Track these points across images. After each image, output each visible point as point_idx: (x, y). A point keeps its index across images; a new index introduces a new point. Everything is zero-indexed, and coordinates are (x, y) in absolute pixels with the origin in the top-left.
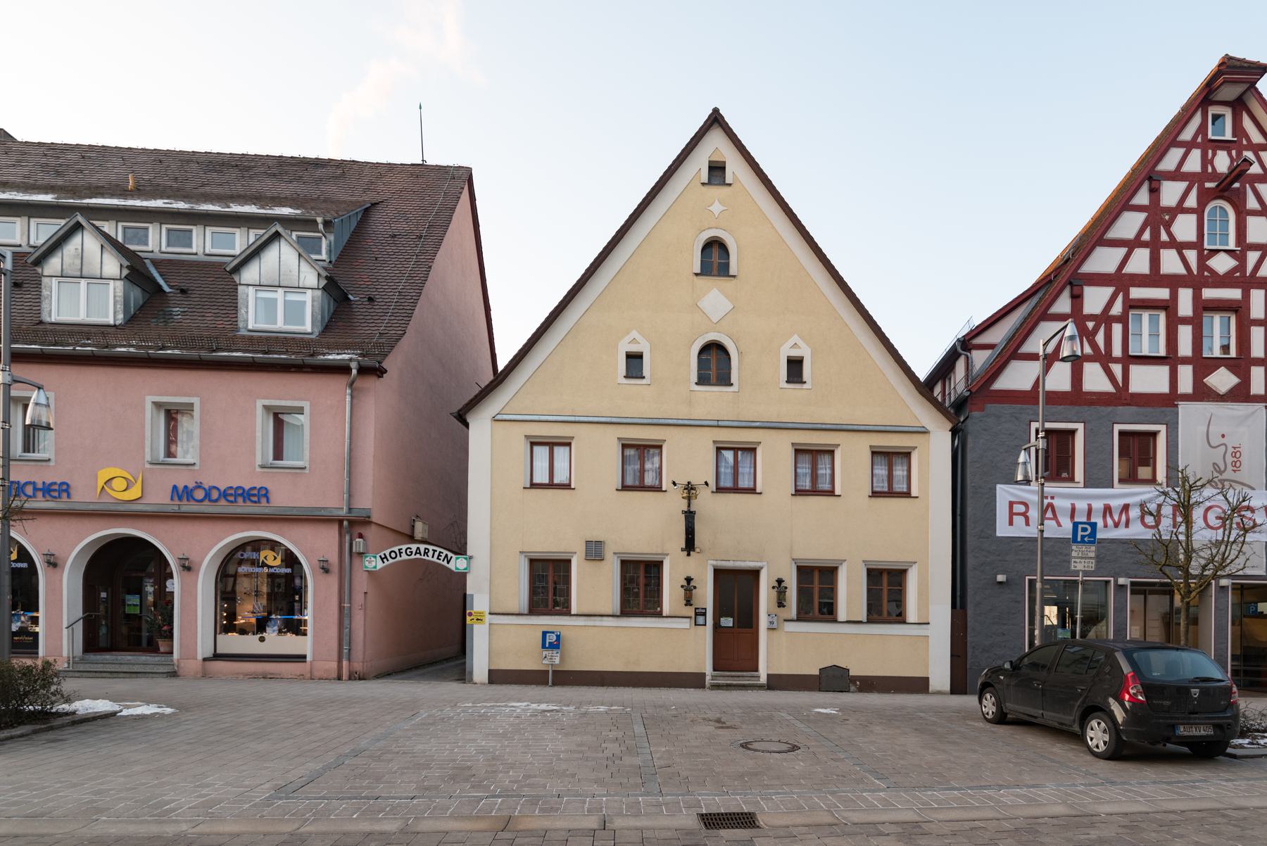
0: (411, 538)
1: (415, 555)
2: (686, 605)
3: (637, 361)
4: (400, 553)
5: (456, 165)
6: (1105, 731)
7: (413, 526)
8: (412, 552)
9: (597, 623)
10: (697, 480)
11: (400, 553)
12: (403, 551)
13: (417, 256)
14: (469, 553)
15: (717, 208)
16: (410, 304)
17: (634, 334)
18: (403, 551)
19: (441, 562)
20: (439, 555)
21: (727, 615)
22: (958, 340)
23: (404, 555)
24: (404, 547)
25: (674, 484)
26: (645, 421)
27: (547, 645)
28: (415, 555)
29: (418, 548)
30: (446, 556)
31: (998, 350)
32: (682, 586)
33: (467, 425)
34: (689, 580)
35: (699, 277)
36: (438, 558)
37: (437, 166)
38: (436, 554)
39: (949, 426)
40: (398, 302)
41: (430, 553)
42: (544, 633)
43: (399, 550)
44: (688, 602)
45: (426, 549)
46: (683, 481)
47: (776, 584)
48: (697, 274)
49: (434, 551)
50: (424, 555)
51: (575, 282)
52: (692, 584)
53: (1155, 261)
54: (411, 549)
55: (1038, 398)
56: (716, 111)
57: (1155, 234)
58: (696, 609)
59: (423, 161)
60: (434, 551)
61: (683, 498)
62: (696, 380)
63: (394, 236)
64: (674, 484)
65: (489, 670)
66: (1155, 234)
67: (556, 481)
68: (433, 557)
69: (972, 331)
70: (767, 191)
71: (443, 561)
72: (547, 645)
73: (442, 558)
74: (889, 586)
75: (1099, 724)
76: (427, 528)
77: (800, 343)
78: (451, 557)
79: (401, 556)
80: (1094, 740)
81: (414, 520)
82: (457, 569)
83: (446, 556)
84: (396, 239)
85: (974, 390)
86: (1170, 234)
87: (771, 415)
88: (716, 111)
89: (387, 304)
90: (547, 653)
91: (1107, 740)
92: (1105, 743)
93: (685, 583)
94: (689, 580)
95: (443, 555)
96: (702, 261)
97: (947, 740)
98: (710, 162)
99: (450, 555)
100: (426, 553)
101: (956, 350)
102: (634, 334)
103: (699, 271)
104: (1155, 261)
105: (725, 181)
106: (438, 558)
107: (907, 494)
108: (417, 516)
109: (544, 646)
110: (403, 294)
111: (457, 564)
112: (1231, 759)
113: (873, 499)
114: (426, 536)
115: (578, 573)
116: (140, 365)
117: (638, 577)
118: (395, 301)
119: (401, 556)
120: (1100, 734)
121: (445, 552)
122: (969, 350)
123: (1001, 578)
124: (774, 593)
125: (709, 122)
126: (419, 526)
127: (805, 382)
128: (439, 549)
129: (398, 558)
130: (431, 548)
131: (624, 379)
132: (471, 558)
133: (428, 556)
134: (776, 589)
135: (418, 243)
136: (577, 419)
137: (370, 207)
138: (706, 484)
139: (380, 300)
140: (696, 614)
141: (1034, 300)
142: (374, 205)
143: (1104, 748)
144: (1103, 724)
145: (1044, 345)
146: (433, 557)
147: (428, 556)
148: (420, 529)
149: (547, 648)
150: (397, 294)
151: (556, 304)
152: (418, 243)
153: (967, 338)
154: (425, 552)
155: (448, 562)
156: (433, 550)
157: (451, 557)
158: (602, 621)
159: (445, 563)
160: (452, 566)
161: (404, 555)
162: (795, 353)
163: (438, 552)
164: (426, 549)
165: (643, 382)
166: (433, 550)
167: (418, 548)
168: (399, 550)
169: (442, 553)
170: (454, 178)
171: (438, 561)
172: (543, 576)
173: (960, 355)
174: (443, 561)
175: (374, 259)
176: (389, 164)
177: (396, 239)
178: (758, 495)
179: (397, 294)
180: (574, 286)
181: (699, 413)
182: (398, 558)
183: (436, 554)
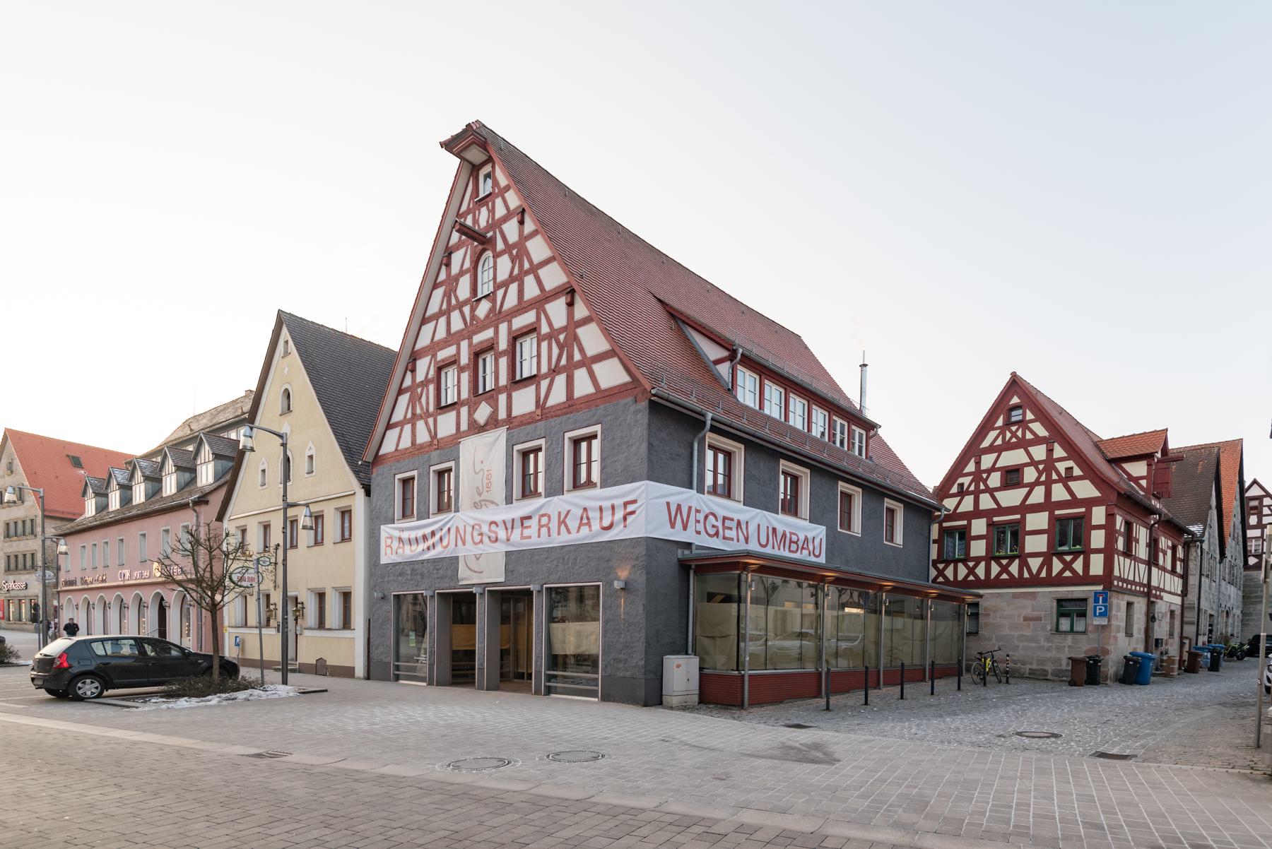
6: (84, 683)
53: (1048, 493)
57: (977, 486)
66: (977, 486)
67: (1184, 625)
75: (80, 688)
80: (93, 691)
86: (986, 485)
91: (89, 680)
92: (92, 683)
97: (61, 802)
104: (1048, 493)
112: (1237, 474)
116: (773, 380)
120: (87, 687)
141: (698, 626)
143: (97, 683)
144: (80, 685)
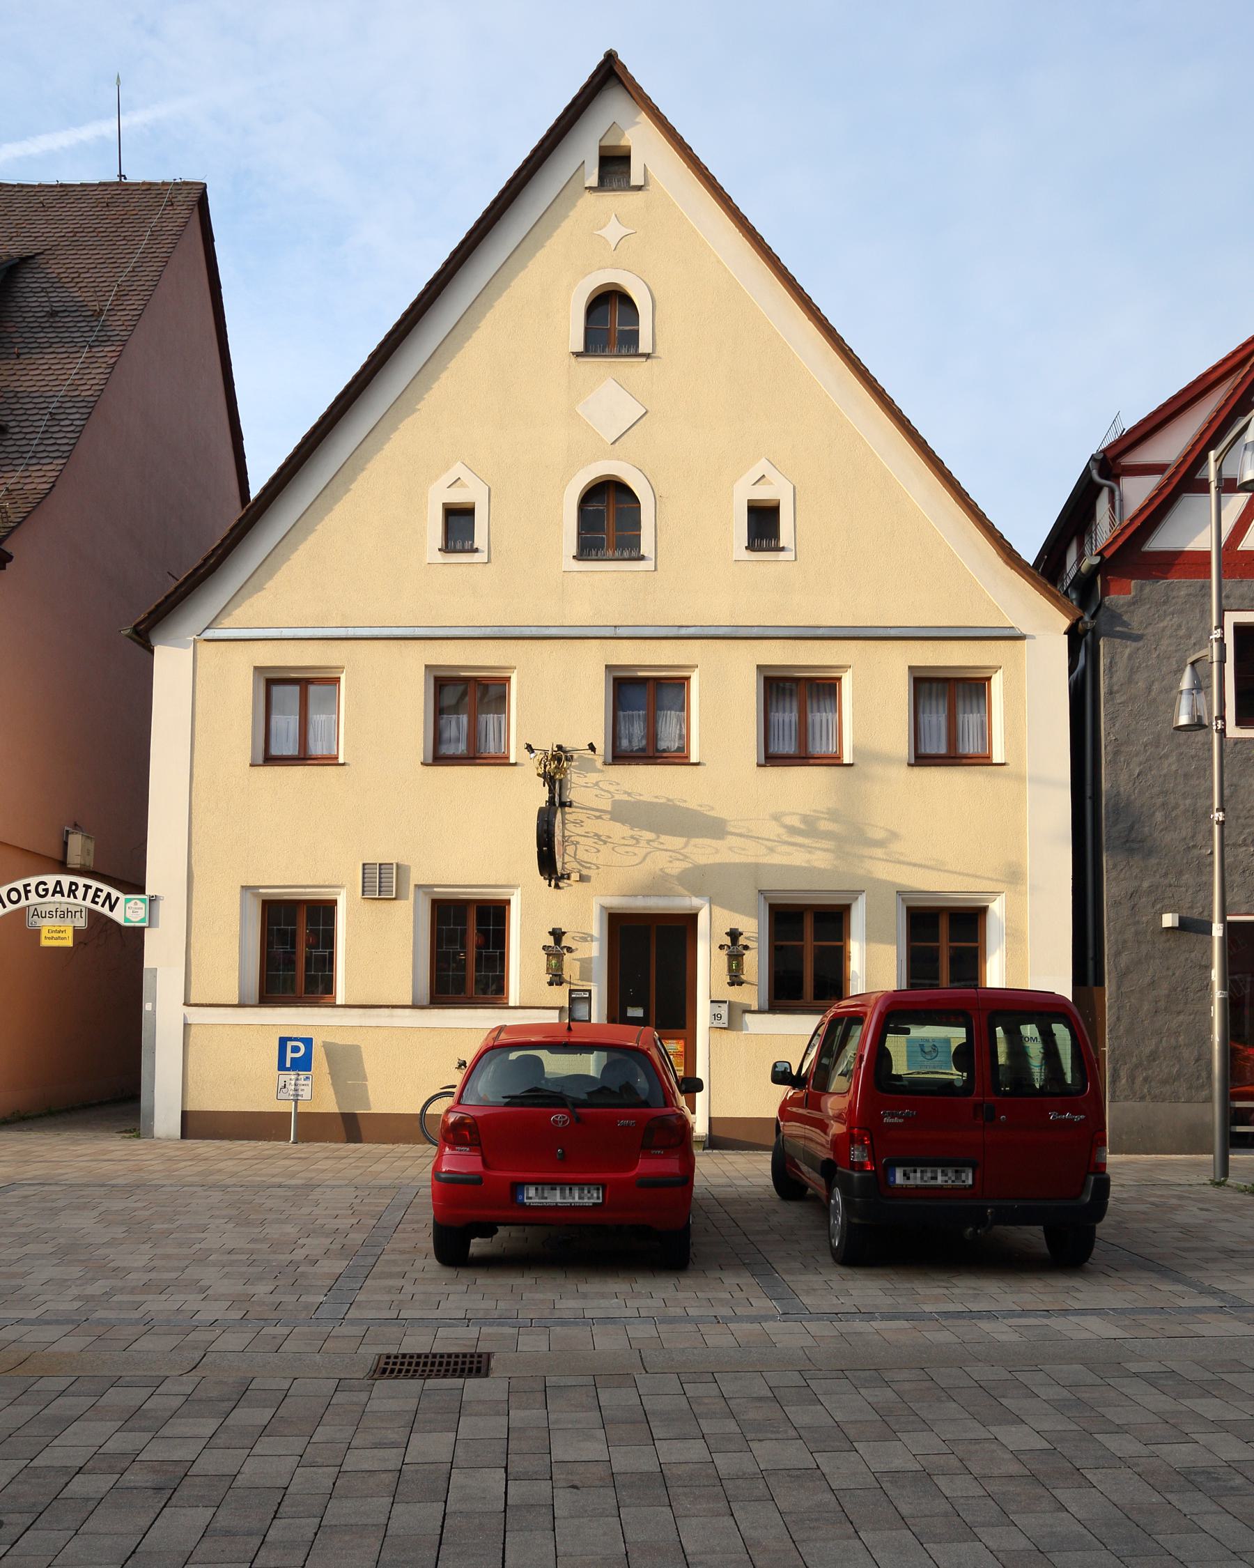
0: (62, 866)
1: (53, 895)
2: (731, 984)
3: (463, 520)
4: (27, 892)
5: (179, 181)
7: (66, 844)
8: (46, 890)
9: (397, 1022)
10: (575, 741)
11: (27, 892)
12: (32, 888)
13: (91, 347)
14: (150, 890)
15: (613, 231)
16: (69, 435)
17: (458, 470)
18: (32, 888)
19: (98, 908)
20: (96, 896)
21: (635, 1005)
22: (1093, 458)
23: (32, 895)
24: (33, 881)
25: (530, 748)
26: (477, 633)
27: (288, 1065)
28: (53, 895)
29: (58, 883)
30: (109, 896)
31: (1168, 473)
32: (544, 948)
33: (152, 652)
34: (557, 935)
35: (580, 359)
36: (93, 901)
37: (144, 184)
38: (91, 893)
39: (1065, 623)
40: (47, 431)
41: (81, 891)
42: (283, 1042)
43: (25, 886)
44: (557, 979)
45: (72, 884)
46: (546, 744)
47: (727, 941)
48: (578, 355)
49: (87, 887)
50: (69, 896)
51: (348, 379)
52: (742, 941)
54: (45, 884)
55: (1210, 563)
56: (611, 57)
58: (571, 991)
59: (120, 176)
60: (87, 887)
61: (539, 775)
62: (574, 551)
63: (53, 314)
64: (530, 748)
65: (184, 1114)
68: (84, 899)
69: (1122, 438)
70: (540, 169)
71: (103, 905)
72: (288, 1065)
73: (100, 900)
74: (951, 941)
76: (91, 846)
77: (772, 474)
78: (118, 899)
79: (27, 898)
81: (67, 831)
82: (126, 920)
83: (109, 896)
84: (57, 319)
85: (1107, 555)
87: (720, 614)
88: (611, 57)
89: (28, 436)
90: (287, 1078)
93: (550, 941)
94: (557, 935)
95: (103, 895)
96: (586, 330)
98: (601, 148)
99: (115, 893)
100: (72, 892)
101: (1091, 481)
102: (458, 470)
103: (580, 347)
105: (629, 182)
106: (93, 901)
107: (983, 760)
108: (76, 825)
109: (282, 1066)
110: (57, 417)
111: (127, 911)
113: (917, 770)
114: (90, 862)
115: (349, 924)
117: (464, 932)
118: (42, 429)
119: (27, 898)
121: (107, 889)
122: (1116, 478)
123: (1168, 920)
124: (723, 957)
125: (597, 79)
126: (76, 843)
127: (782, 549)
128: (95, 884)
129: (23, 903)
130: (81, 881)
131: (574, 562)
132: (153, 900)
133: (75, 897)
134: (725, 952)
135: (95, 324)
136: (351, 632)
137: (18, 264)
138: (592, 748)
139: (17, 430)
140: (572, 1000)
142: (25, 260)
145: (1216, 461)
146: (84, 899)
147: (75, 897)
148: (78, 848)
149: (288, 1069)
150: (47, 417)
151: (314, 420)
152: (95, 324)
153: (1109, 455)
154: (70, 891)
155: (112, 908)
156: (85, 886)
157: (118, 899)
158: (392, 1016)
159: (106, 910)
160: (118, 916)
161: (32, 895)
162: (763, 494)
163: (93, 889)
164: (72, 884)
165: (476, 557)
166: (85, 886)
167: (58, 883)
168: (25, 886)
169: (101, 891)
170: (172, 205)
171: (93, 906)
172: (285, 932)
173: (1099, 488)
174: (103, 905)
175: (15, 356)
176: (62, 185)
177: (57, 319)
178: (694, 768)
179: (47, 417)
180: (348, 387)
181: (579, 614)
182: (23, 903)
183: (91, 893)
